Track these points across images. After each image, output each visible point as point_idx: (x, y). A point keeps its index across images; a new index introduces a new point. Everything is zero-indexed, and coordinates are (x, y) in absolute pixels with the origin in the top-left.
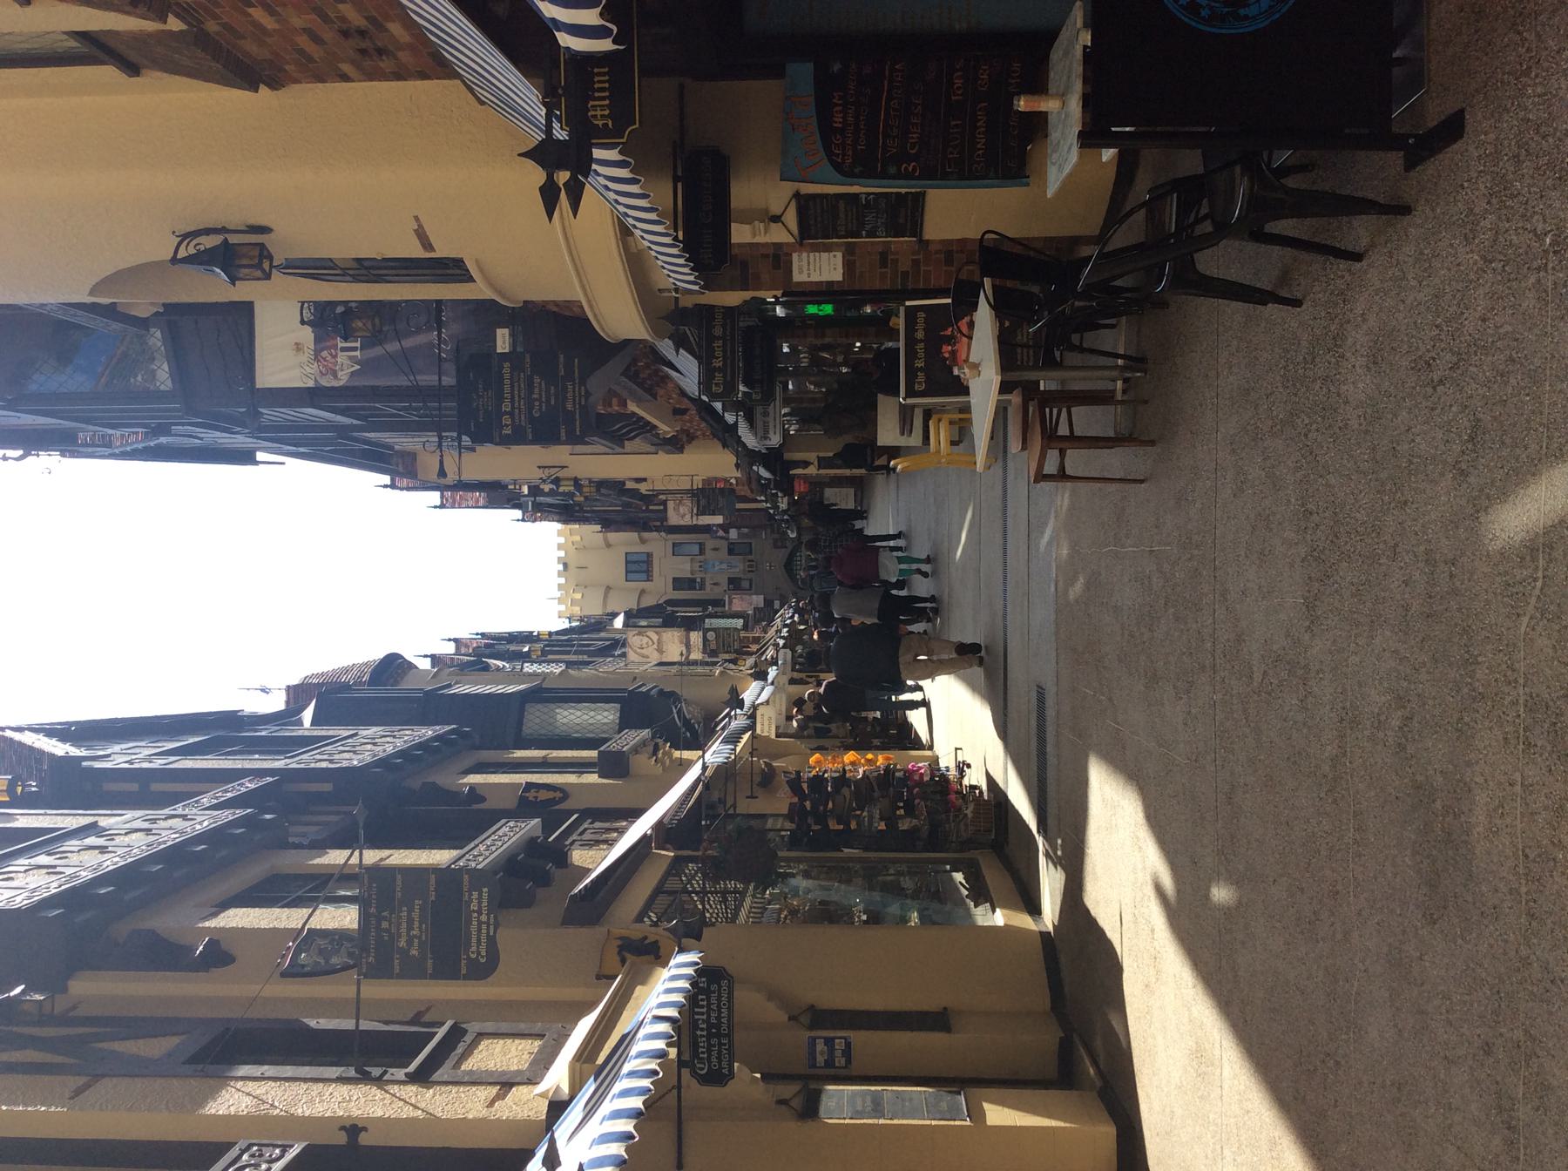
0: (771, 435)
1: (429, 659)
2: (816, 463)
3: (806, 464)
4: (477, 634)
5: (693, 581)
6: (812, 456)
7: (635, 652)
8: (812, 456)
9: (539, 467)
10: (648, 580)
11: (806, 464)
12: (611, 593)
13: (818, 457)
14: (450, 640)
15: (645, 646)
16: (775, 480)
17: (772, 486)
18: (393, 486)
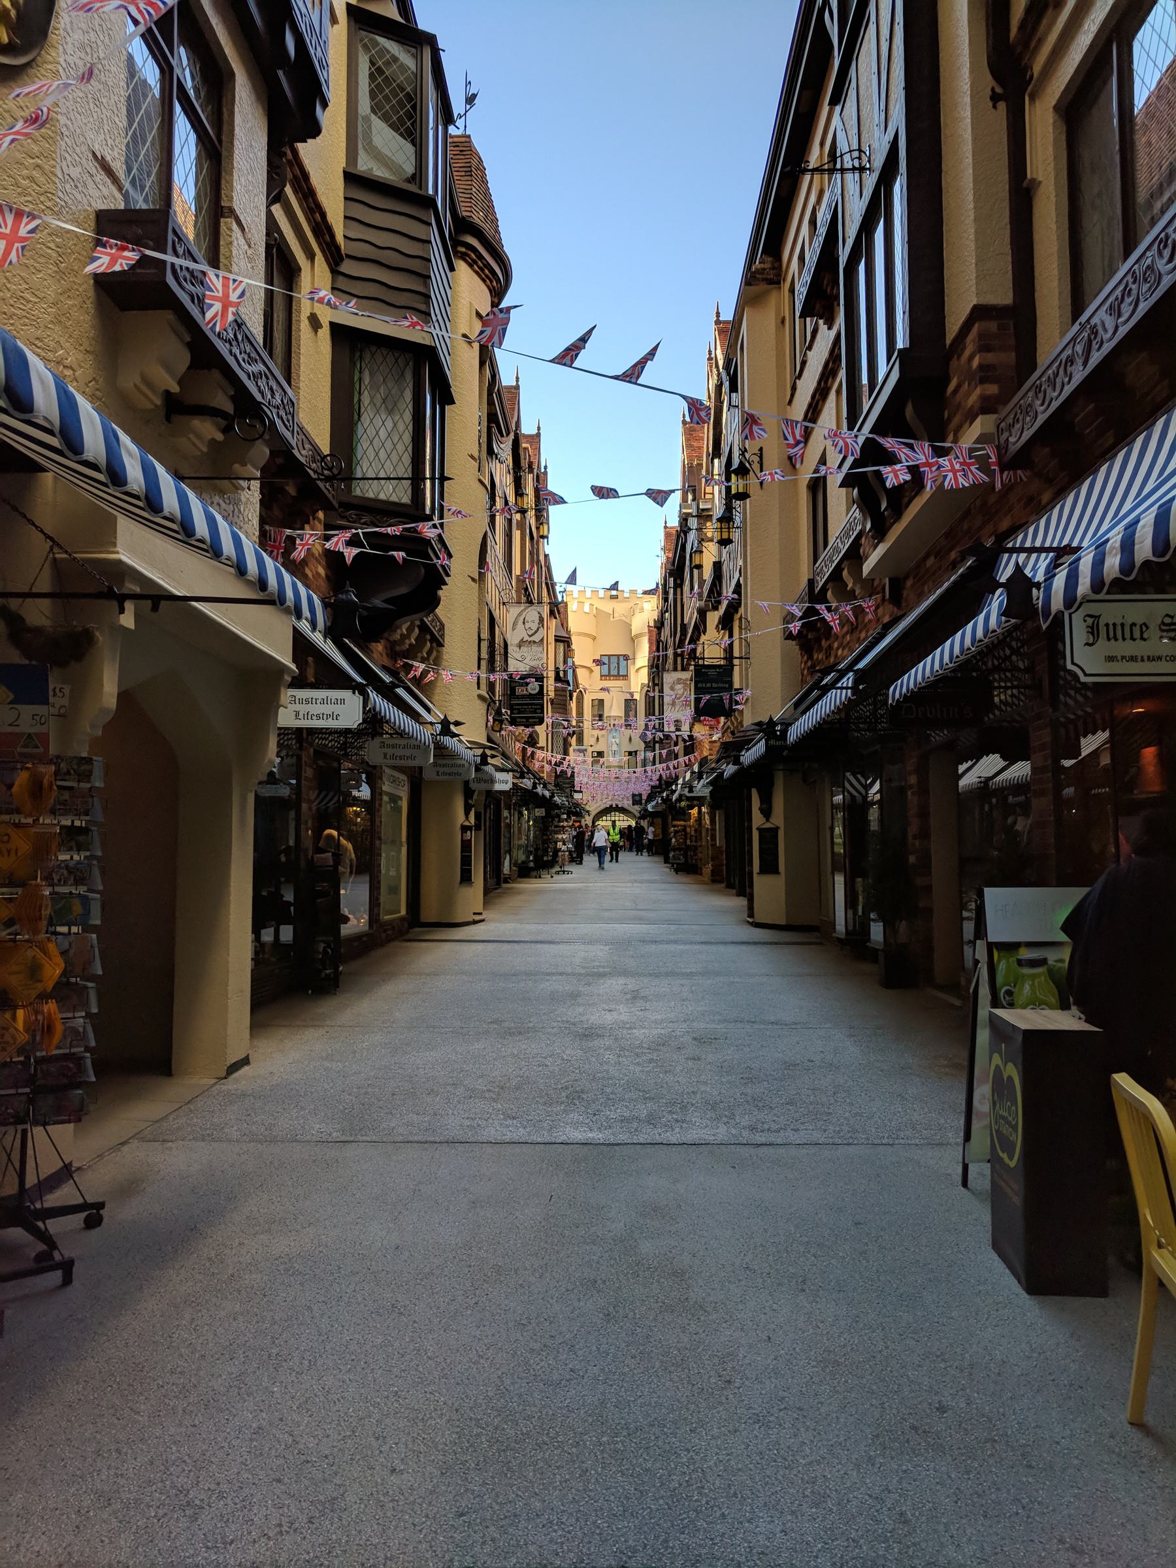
0: (1104, 646)
1: (515, 384)
2: (768, 825)
3: (767, 812)
4: (546, 467)
5: (601, 717)
6: (778, 819)
7: (520, 614)
8: (778, 819)
9: (761, 449)
10: (601, 676)
11: (767, 812)
12: (589, 640)
13: (777, 828)
14: (539, 428)
15: (527, 625)
16: (786, 747)
17: (772, 742)
18: (667, 535)
